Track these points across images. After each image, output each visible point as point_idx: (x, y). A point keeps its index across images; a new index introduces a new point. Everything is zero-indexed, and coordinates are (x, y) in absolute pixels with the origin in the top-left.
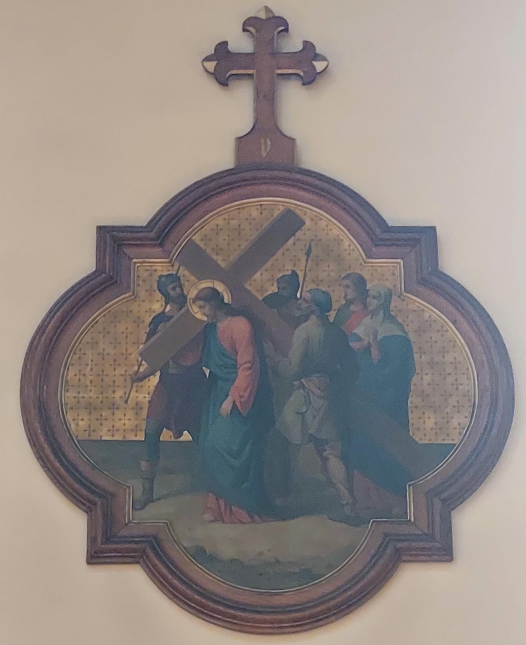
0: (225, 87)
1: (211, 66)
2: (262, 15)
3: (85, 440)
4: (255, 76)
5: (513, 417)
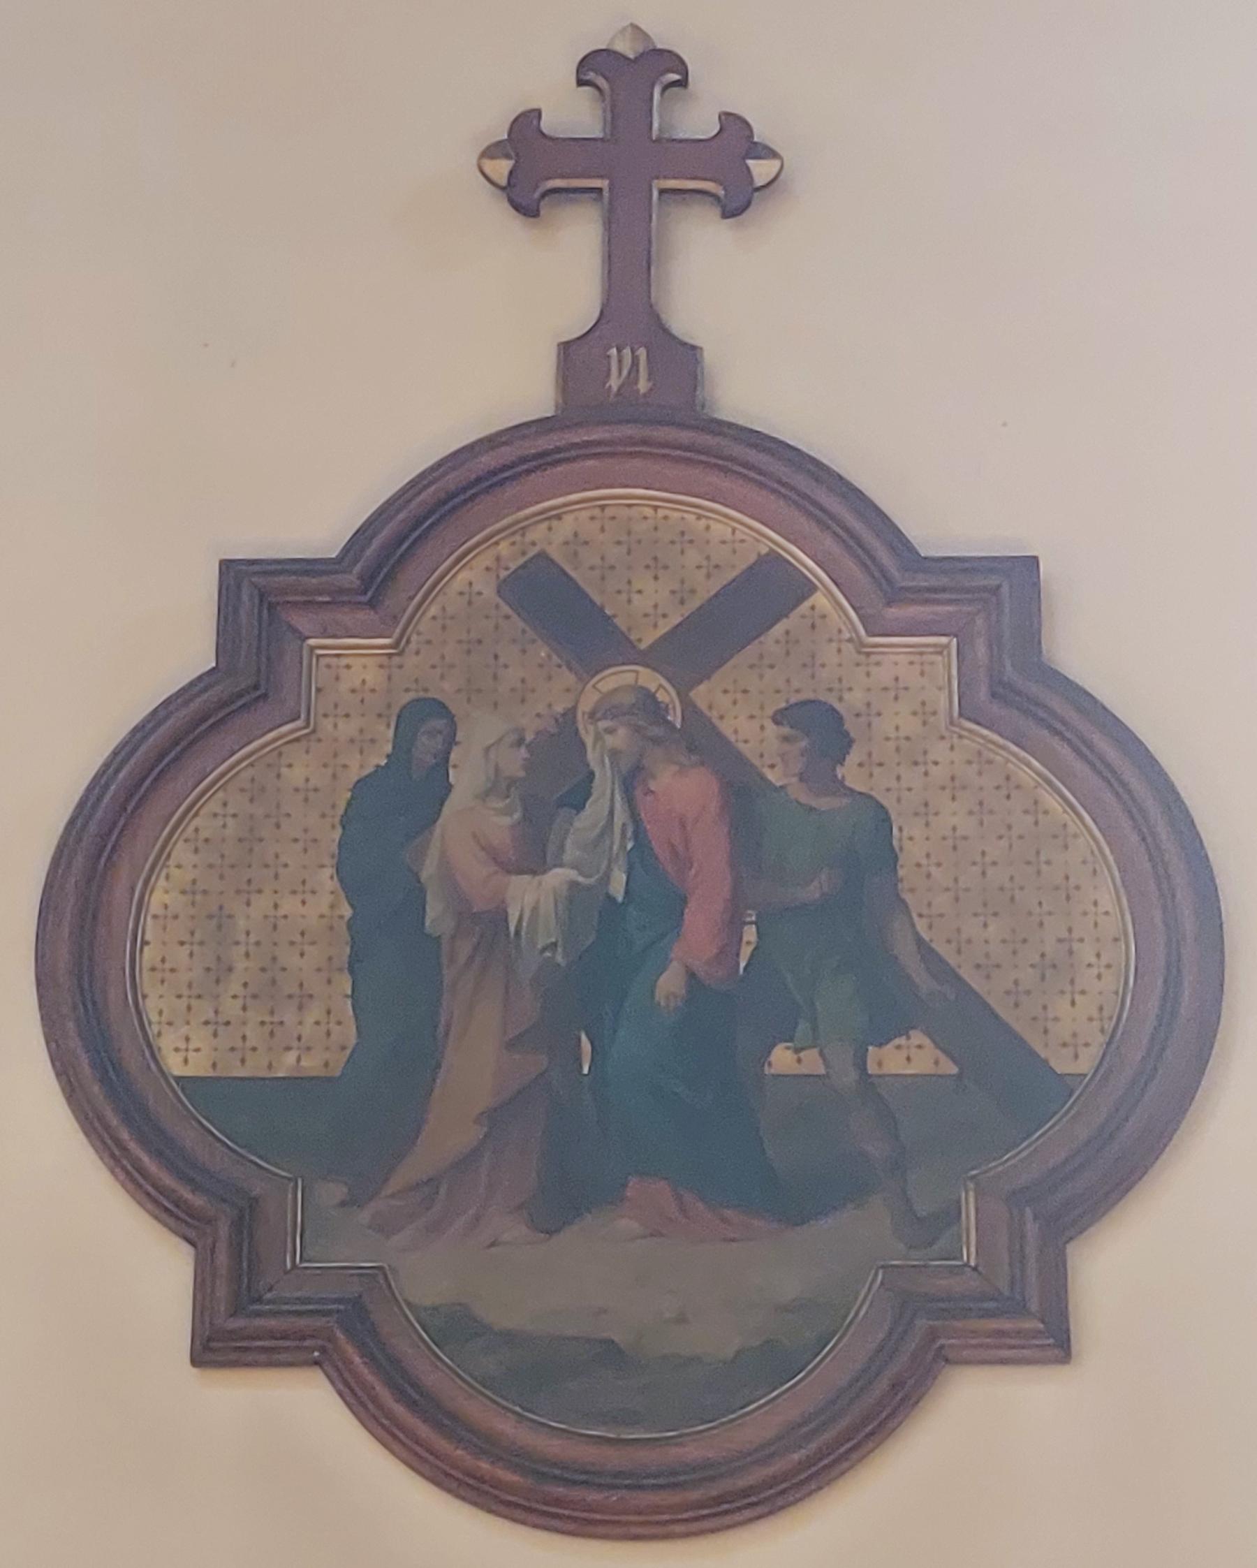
0: (532, 220)
1: (501, 168)
2: (626, 47)
3: (783, 1076)
4: (606, 194)
5: (1221, 1002)
